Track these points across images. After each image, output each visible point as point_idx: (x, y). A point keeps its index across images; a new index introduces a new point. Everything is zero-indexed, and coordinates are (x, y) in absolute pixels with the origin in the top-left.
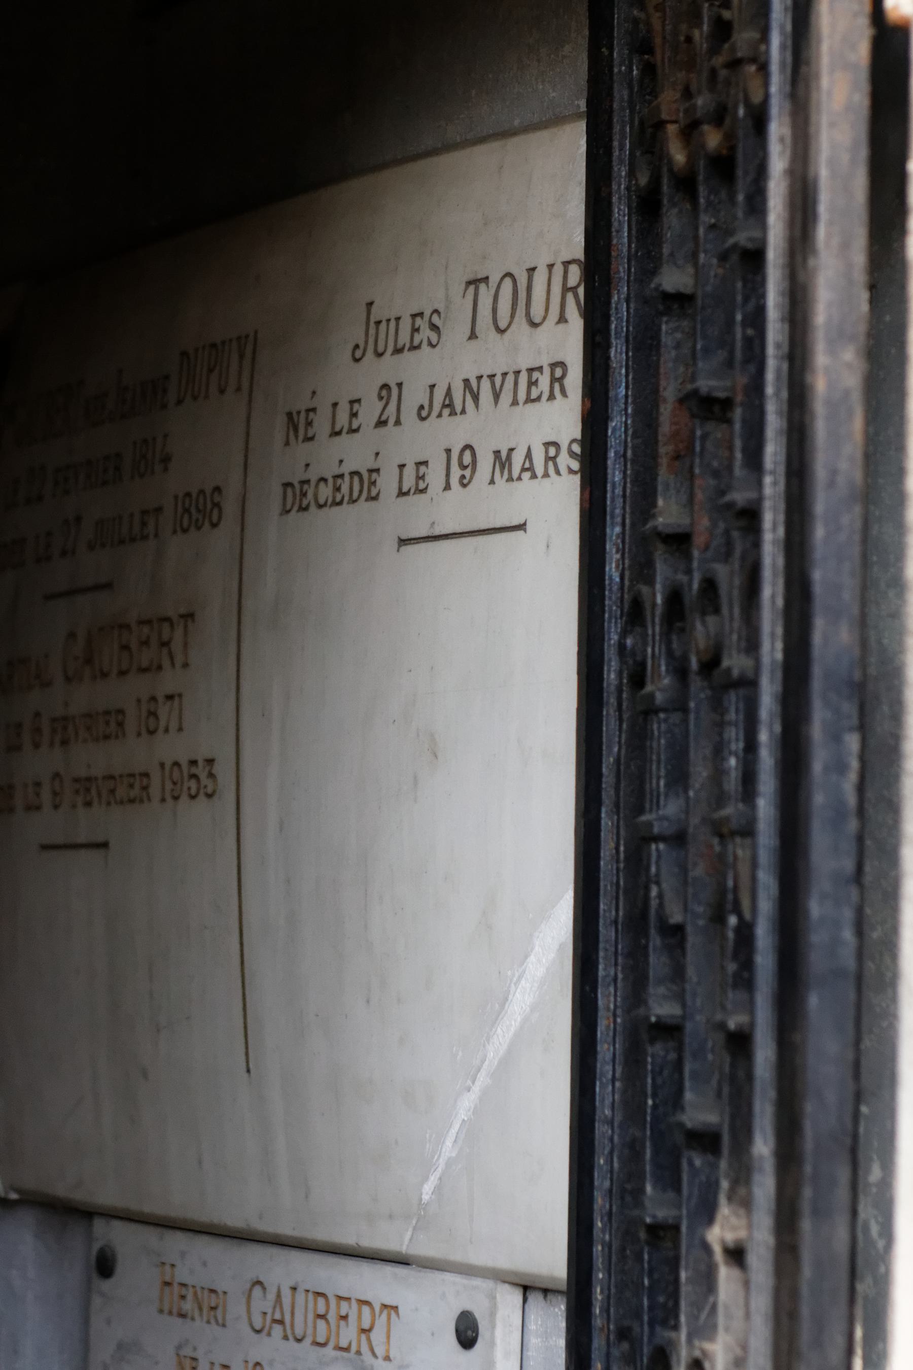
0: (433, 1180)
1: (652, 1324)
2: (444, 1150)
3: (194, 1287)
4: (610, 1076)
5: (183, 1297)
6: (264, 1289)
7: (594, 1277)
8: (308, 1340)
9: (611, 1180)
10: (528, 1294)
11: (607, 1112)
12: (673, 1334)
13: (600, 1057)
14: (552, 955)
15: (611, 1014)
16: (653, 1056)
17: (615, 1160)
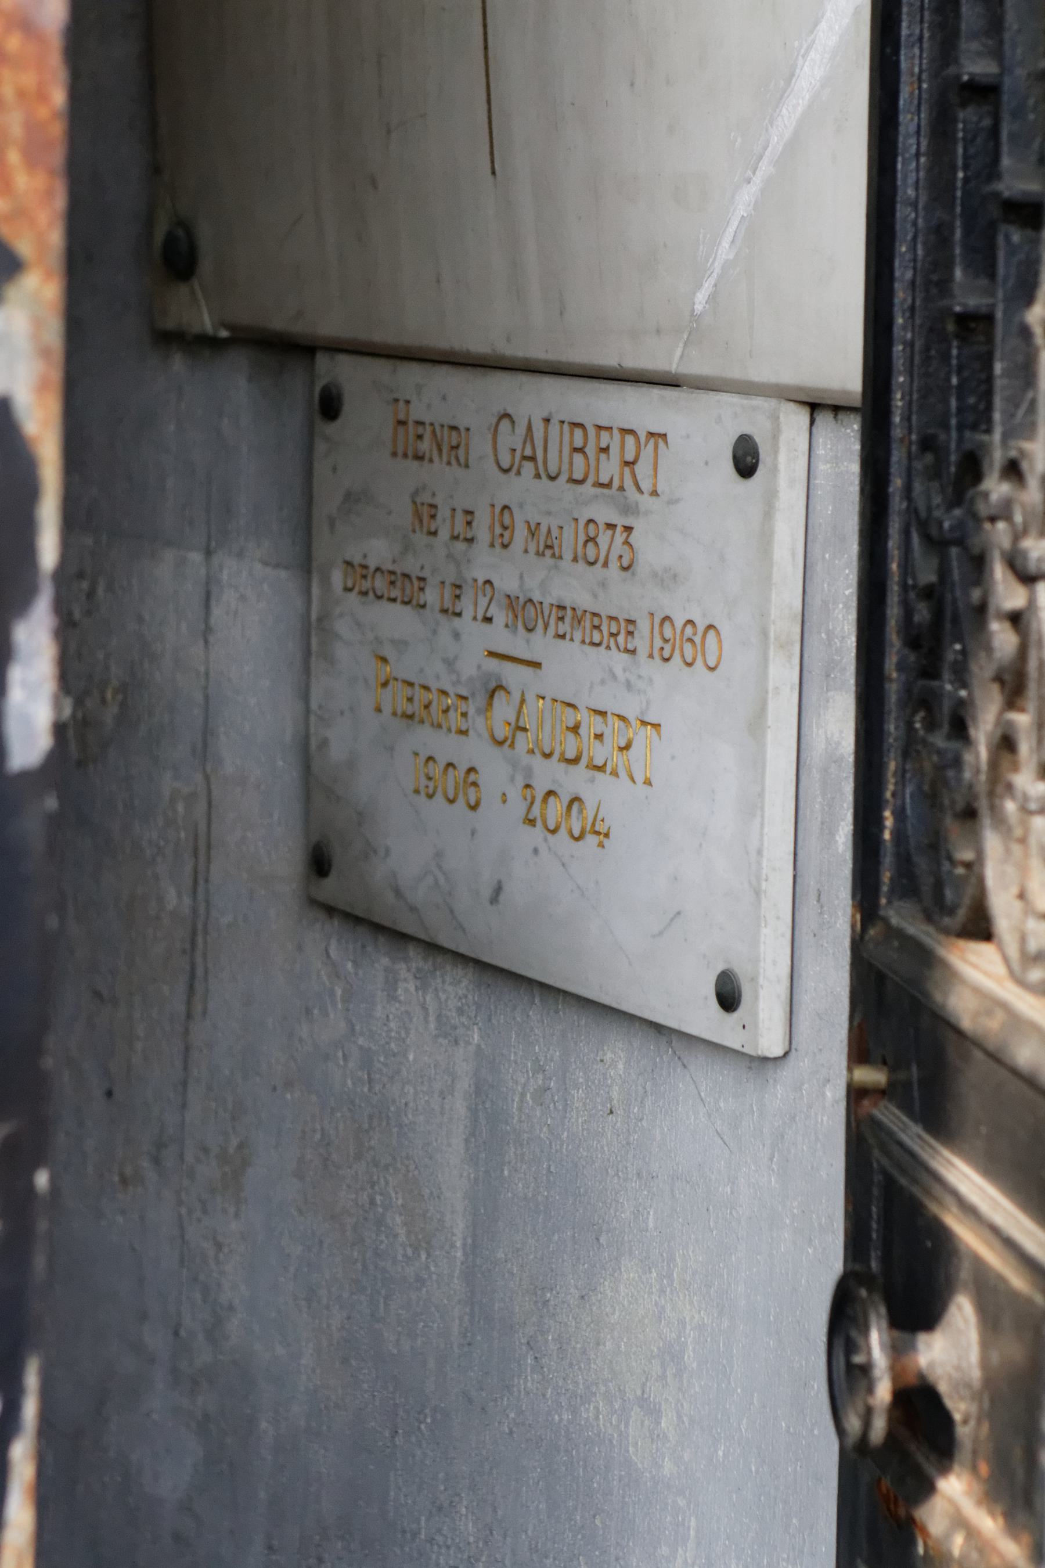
0: (708, 287)
1: (961, 427)
2: (720, 252)
3: (432, 424)
4: (913, 150)
5: (420, 437)
6: (513, 422)
7: (893, 382)
8: (564, 478)
9: (915, 269)
10: (815, 415)
11: (911, 192)
12: (985, 437)
13: (902, 129)
14: (846, 21)
15: (915, 78)
16: (964, 122)
17: (919, 247)
